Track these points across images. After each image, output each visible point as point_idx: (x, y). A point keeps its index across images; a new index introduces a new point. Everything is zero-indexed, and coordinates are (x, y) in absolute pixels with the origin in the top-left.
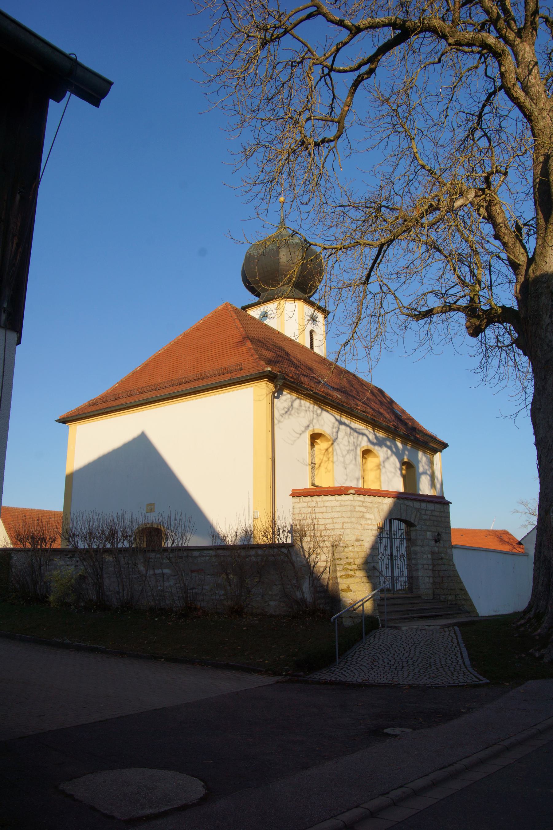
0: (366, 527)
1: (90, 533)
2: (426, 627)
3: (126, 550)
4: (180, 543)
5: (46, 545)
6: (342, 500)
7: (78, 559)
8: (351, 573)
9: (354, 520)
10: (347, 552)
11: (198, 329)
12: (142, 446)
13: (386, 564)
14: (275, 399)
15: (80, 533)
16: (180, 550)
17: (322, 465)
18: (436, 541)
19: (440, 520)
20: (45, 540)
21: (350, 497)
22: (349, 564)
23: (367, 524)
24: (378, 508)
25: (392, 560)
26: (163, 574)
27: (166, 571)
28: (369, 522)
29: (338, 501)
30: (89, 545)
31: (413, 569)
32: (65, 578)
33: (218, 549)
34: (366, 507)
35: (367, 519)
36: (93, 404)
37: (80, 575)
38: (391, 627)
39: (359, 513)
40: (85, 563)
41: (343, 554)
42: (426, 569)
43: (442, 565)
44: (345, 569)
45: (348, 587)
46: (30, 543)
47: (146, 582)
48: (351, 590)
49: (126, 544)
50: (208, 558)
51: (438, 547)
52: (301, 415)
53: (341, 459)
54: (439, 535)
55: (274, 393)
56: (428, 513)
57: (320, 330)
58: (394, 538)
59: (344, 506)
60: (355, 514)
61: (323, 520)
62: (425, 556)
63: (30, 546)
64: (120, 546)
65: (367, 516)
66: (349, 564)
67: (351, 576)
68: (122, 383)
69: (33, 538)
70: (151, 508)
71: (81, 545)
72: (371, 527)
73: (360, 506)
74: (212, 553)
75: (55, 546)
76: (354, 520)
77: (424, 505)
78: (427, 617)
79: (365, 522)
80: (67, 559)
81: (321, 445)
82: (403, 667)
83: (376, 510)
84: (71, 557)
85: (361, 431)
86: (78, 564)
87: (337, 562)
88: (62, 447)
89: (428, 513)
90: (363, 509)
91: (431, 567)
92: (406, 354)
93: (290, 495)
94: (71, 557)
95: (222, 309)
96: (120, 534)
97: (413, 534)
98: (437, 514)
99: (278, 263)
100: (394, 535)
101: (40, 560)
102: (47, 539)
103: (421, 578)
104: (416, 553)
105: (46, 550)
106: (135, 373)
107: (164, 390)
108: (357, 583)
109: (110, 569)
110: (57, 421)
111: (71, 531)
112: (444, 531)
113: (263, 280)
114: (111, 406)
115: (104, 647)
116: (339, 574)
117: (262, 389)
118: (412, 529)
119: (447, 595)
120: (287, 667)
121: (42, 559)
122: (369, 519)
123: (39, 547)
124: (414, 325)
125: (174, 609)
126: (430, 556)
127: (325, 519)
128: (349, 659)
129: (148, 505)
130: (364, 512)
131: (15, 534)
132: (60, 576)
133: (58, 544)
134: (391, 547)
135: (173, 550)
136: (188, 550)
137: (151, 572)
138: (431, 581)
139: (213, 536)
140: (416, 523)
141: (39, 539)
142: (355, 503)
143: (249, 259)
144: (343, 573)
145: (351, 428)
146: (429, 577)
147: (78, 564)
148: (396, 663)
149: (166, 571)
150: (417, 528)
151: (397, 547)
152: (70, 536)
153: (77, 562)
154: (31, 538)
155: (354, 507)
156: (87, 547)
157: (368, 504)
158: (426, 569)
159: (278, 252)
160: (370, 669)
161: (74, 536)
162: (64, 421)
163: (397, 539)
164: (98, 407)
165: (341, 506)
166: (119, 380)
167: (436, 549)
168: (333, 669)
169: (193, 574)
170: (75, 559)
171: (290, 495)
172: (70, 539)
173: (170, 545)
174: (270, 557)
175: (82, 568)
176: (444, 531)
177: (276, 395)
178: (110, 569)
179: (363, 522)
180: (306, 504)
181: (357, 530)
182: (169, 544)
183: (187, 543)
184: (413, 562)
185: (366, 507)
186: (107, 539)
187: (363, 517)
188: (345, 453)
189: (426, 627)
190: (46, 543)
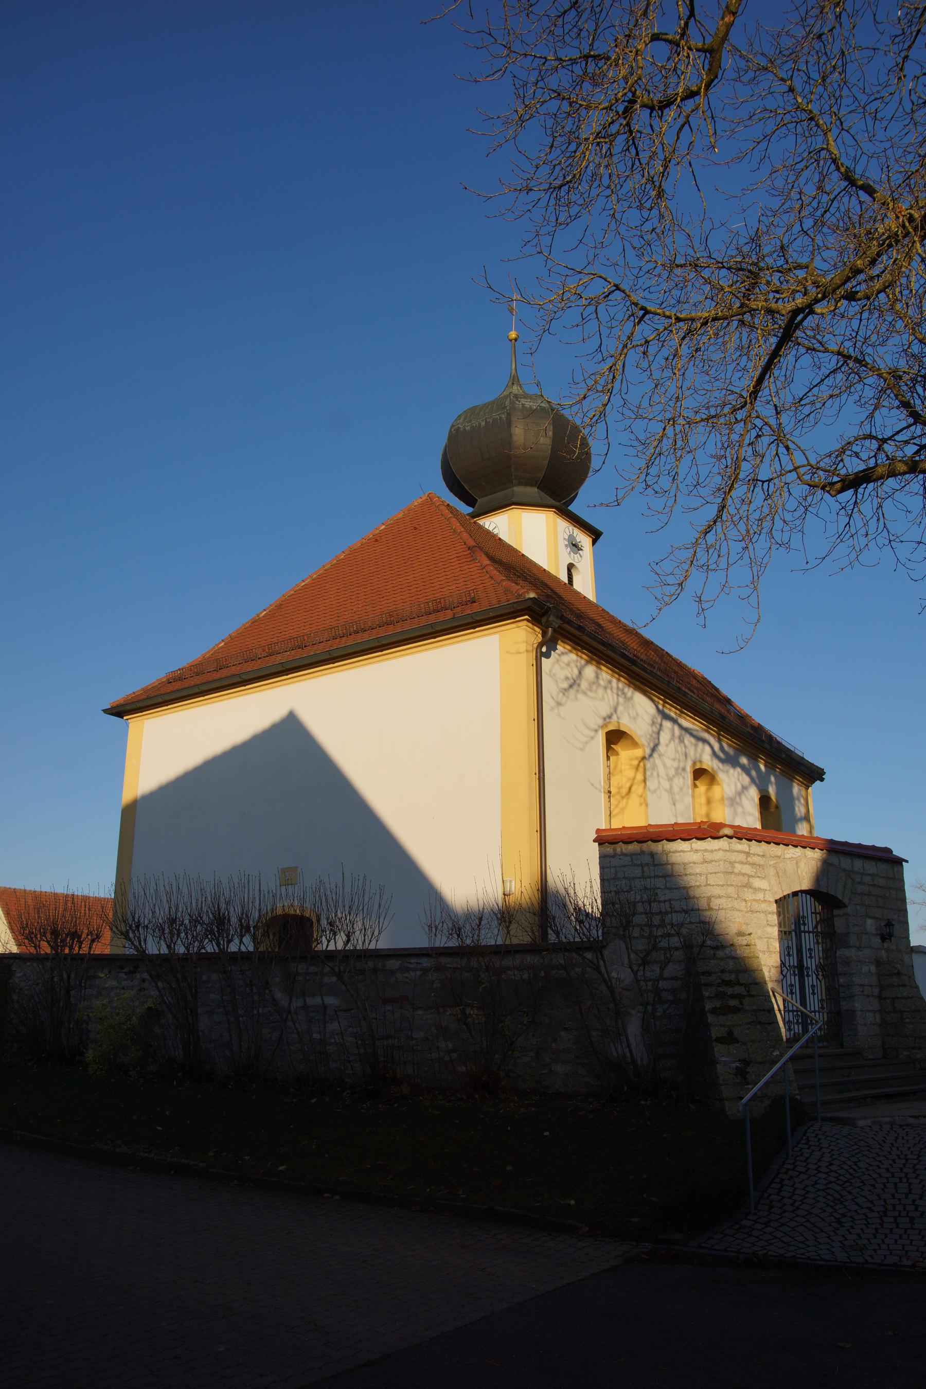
0: (756, 906)
1: (172, 921)
2: (912, 1121)
3: (245, 957)
4: (360, 942)
5: (80, 947)
6: (706, 850)
7: (146, 976)
8: (733, 1003)
9: (731, 890)
10: (721, 959)
11: (376, 541)
12: (290, 729)
13: (791, 985)
14: (543, 659)
15: (150, 922)
16: (359, 957)
17: (633, 789)
18: (883, 939)
19: (887, 895)
20: (80, 937)
21: (722, 843)
22: (728, 984)
23: (757, 901)
24: (775, 868)
25: (801, 976)
26: (325, 1007)
27: (329, 1000)
28: (760, 896)
29: (697, 851)
30: (169, 947)
31: (842, 995)
32: (118, 1014)
33: (441, 954)
34: (753, 865)
35: (757, 890)
36: (176, 678)
37: (150, 1008)
38: (831, 1119)
39: (741, 878)
40: (160, 984)
41: (713, 962)
42: (868, 996)
43: (899, 986)
44: (720, 995)
45: (730, 1034)
46: (48, 942)
47: (290, 1024)
48: (736, 1041)
49: (248, 944)
50: (418, 973)
51: (887, 950)
52: (590, 697)
53: (666, 784)
54: (889, 924)
55: (541, 645)
56: (867, 879)
57: (585, 562)
58: (805, 932)
59: (711, 862)
60: (733, 879)
61: (667, 891)
62: (865, 969)
63: (48, 950)
64: (233, 948)
65: (757, 883)
66: (728, 984)
67: (735, 1010)
68: (231, 640)
69: (55, 933)
70: (288, 877)
71: (154, 947)
72: (763, 906)
73: (742, 863)
74: (426, 962)
75: (100, 949)
76: (731, 890)
77: (858, 864)
78: (890, 1097)
79: (754, 897)
80: (123, 975)
81: (626, 755)
82: (912, 1220)
83: (772, 872)
84: (130, 972)
85: (695, 733)
86: (146, 985)
87: (703, 979)
88: (116, 758)
89: (867, 879)
90: (747, 869)
91: (876, 992)
92: (809, 566)
93: (594, 841)
94: (130, 972)
95: (422, 504)
96: (234, 920)
97: (839, 924)
98: (882, 882)
99: (508, 441)
100: (804, 924)
101: (69, 976)
102: (84, 936)
103: (859, 1013)
104: (847, 962)
105: (80, 958)
106: (256, 622)
107: (315, 647)
108: (747, 1024)
109: (212, 996)
110: (106, 711)
111: (134, 918)
112: (895, 917)
113: (483, 472)
114: (211, 679)
115: (204, 1165)
116: (708, 1006)
117: (520, 635)
118: (836, 912)
119: (913, 1048)
120: (636, 1220)
121: (73, 975)
122: (760, 889)
123: (67, 951)
124: (829, 506)
125: (347, 1080)
126: (873, 968)
127: (670, 889)
128: (772, 1197)
129: (284, 871)
130: (749, 876)
131: (21, 928)
132: (108, 1009)
133: (105, 947)
134: (799, 951)
135: (346, 956)
136: (377, 956)
137: (299, 1003)
138: (878, 1020)
139: (430, 927)
140: (846, 901)
141: (67, 935)
142: (733, 857)
143: (455, 437)
144: (717, 1004)
145: (681, 726)
146: (874, 1011)
147: (146, 985)
148: (890, 1207)
149: (329, 1000)
150: (849, 910)
151: (810, 949)
152: (131, 927)
153: (144, 981)
154: (51, 934)
155: (732, 863)
156: (164, 950)
157: (756, 859)
158: (868, 996)
159: (509, 423)
160: (836, 1225)
161: (138, 927)
162: (120, 711)
163: (809, 932)
164: (186, 684)
165: (705, 862)
166: (225, 635)
167: (884, 954)
168: (746, 1223)
169: (389, 1008)
170: (138, 975)
171: (594, 841)
172: (131, 935)
173: (340, 946)
174: (554, 972)
175: (155, 993)
176: (895, 917)
177: (544, 649)
178: (212, 996)
179: (749, 895)
180: (629, 858)
181: (738, 913)
182: (339, 943)
183: (374, 942)
184: (841, 980)
185: (753, 865)
186: (209, 932)
187: (748, 885)
188: (672, 772)
189: (912, 1121)
190: (81, 943)
